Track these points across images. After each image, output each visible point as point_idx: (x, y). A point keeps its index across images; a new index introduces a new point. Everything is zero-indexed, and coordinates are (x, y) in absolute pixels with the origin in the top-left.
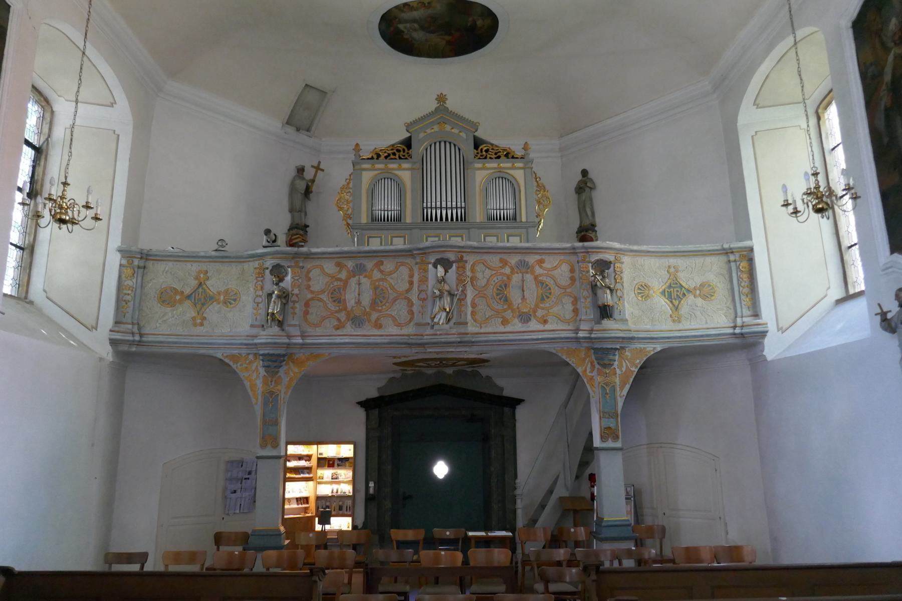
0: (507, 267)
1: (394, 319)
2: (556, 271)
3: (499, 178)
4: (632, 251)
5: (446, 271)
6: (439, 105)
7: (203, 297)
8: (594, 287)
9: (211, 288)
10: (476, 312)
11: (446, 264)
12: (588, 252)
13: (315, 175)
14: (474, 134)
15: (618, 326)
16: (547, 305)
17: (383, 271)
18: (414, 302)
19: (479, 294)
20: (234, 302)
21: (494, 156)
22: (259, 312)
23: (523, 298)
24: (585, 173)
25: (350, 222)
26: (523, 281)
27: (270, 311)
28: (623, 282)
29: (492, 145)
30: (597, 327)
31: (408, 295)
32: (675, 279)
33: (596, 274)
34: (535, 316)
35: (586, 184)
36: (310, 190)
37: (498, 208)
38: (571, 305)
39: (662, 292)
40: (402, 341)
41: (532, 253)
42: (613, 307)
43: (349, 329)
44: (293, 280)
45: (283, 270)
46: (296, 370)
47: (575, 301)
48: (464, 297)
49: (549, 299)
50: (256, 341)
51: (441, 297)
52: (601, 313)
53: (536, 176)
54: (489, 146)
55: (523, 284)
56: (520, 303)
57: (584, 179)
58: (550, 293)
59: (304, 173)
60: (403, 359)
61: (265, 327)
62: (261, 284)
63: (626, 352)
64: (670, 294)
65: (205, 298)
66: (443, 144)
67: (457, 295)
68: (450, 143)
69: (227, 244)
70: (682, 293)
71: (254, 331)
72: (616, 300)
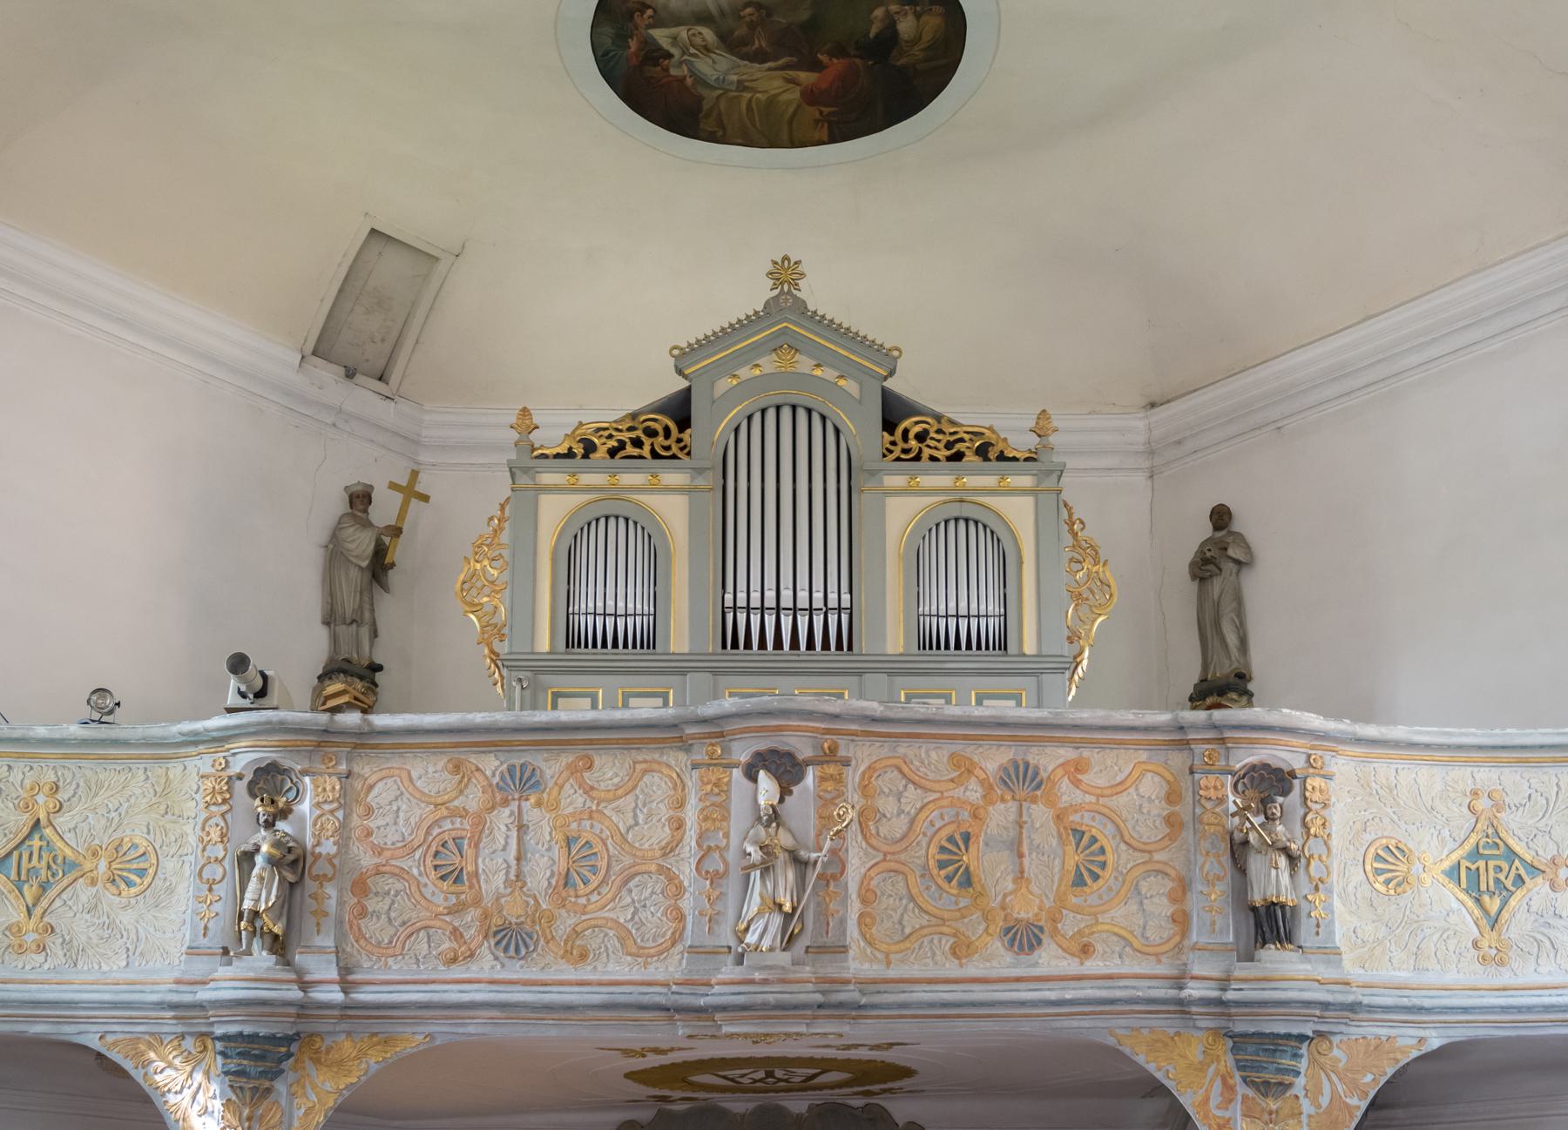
0: (973, 779)
1: (624, 937)
2: (1122, 800)
3: (956, 520)
4: (1359, 741)
5: (785, 792)
6: (776, 292)
7: (44, 863)
8: (1239, 850)
9: (67, 836)
10: (873, 918)
11: (786, 769)
12: (1222, 741)
13: (402, 515)
14: (884, 384)
15: (1309, 967)
16: (1093, 900)
17: (592, 788)
18: (686, 883)
19: (884, 860)
20: (138, 880)
21: (943, 453)
22: (218, 907)
23: (1020, 875)
24: (1221, 517)
25: (503, 648)
26: (1020, 825)
27: (247, 904)
28: (1329, 835)
29: (938, 418)
30: (1242, 970)
31: (669, 862)
32: (1490, 831)
33: (1247, 808)
34: (1055, 932)
35: (1226, 549)
36: (388, 560)
37: (952, 611)
38: (1165, 901)
39: (1452, 868)
40: (646, 999)
41: (1051, 740)
42: (1294, 909)
43: (486, 964)
44: (318, 812)
45: (289, 784)
46: (329, 1086)
47: (1184, 886)
48: (839, 870)
49: (1101, 882)
50: (204, 995)
51: (766, 869)
52: (1258, 925)
53: (1070, 515)
54: (929, 420)
55: (1021, 833)
56: (1011, 893)
57: (1219, 534)
58: (1103, 865)
59: (371, 509)
60: (653, 1061)
61: (232, 954)
62: (222, 824)
63: (1331, 1048)
64: (1475, 876)
65: (49, 867)
66: (786, 414)
67: (816, 862)
68: (809, 411)
69: (118, 704)
70: (1512, 875)
71: (200, 967)
72: (1305, 888)
